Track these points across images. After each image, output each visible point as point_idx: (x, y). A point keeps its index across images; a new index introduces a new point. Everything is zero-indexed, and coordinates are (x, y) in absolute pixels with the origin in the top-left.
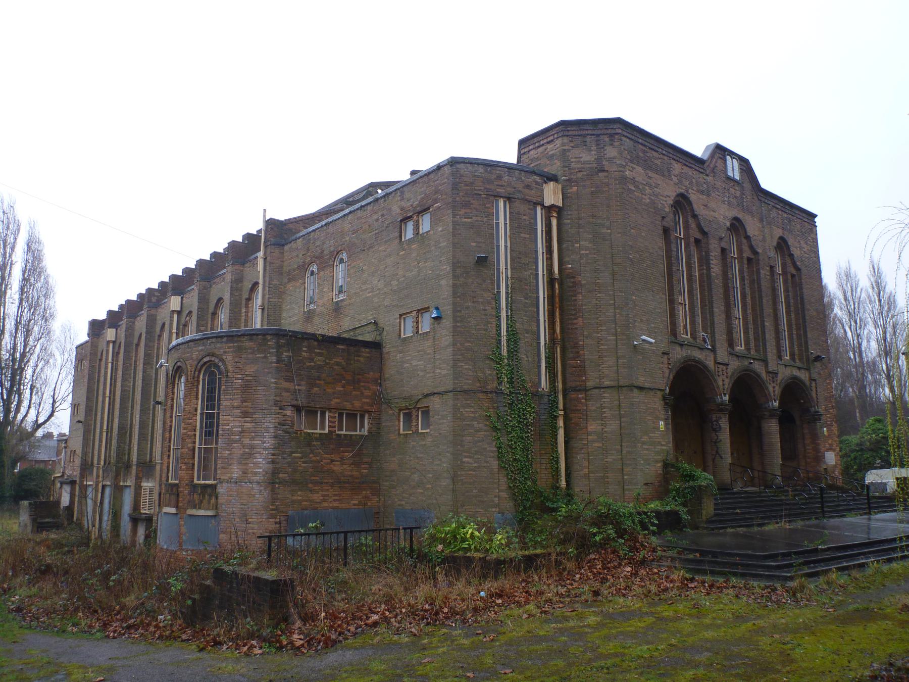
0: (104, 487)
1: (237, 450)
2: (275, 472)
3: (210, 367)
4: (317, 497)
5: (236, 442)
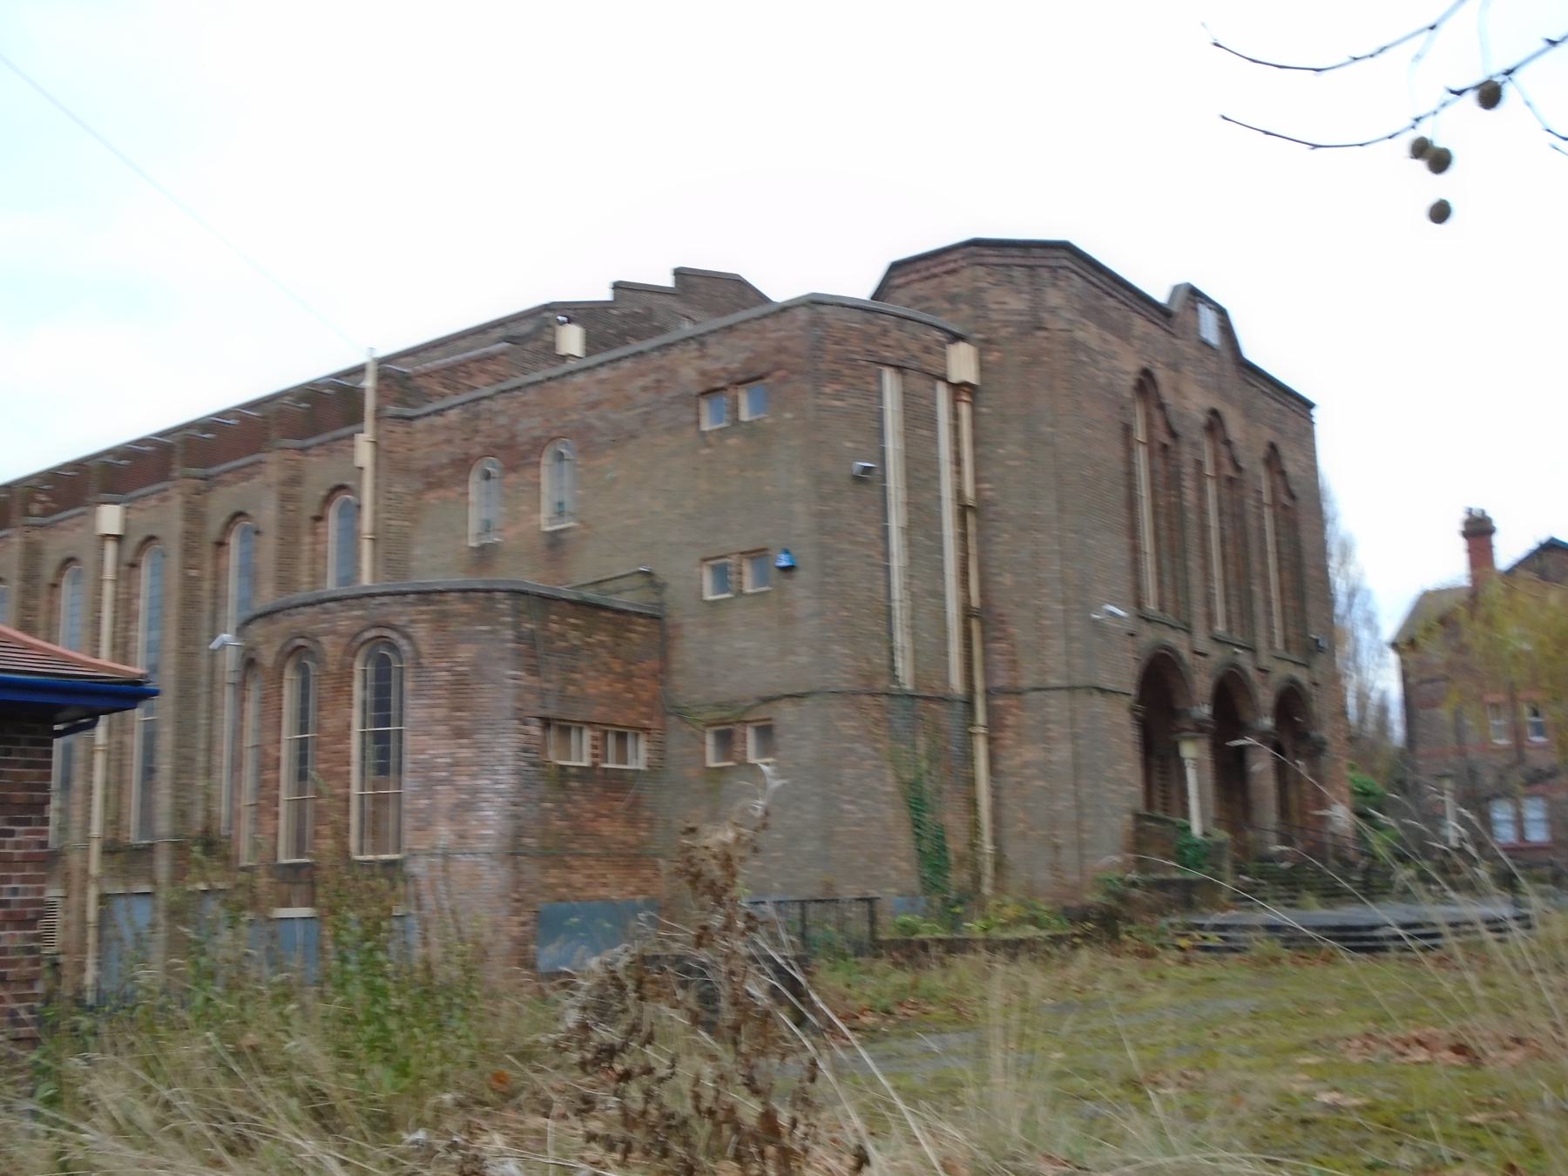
1: (446, 797)
2: (518, 835)
4: (577, 879)
5: (441, 782)
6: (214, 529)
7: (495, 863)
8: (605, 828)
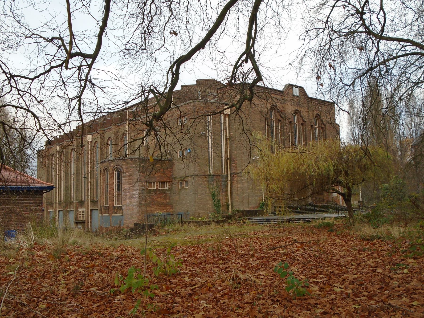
0: (59, 211)
2: (140, 202)
3: (117, 169)
4: (153, 209)
6: (106, 140)
7: (210, 195)
8: (159, 200)
